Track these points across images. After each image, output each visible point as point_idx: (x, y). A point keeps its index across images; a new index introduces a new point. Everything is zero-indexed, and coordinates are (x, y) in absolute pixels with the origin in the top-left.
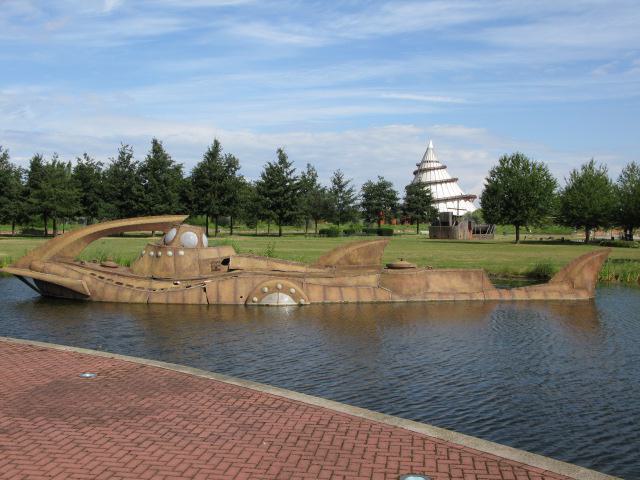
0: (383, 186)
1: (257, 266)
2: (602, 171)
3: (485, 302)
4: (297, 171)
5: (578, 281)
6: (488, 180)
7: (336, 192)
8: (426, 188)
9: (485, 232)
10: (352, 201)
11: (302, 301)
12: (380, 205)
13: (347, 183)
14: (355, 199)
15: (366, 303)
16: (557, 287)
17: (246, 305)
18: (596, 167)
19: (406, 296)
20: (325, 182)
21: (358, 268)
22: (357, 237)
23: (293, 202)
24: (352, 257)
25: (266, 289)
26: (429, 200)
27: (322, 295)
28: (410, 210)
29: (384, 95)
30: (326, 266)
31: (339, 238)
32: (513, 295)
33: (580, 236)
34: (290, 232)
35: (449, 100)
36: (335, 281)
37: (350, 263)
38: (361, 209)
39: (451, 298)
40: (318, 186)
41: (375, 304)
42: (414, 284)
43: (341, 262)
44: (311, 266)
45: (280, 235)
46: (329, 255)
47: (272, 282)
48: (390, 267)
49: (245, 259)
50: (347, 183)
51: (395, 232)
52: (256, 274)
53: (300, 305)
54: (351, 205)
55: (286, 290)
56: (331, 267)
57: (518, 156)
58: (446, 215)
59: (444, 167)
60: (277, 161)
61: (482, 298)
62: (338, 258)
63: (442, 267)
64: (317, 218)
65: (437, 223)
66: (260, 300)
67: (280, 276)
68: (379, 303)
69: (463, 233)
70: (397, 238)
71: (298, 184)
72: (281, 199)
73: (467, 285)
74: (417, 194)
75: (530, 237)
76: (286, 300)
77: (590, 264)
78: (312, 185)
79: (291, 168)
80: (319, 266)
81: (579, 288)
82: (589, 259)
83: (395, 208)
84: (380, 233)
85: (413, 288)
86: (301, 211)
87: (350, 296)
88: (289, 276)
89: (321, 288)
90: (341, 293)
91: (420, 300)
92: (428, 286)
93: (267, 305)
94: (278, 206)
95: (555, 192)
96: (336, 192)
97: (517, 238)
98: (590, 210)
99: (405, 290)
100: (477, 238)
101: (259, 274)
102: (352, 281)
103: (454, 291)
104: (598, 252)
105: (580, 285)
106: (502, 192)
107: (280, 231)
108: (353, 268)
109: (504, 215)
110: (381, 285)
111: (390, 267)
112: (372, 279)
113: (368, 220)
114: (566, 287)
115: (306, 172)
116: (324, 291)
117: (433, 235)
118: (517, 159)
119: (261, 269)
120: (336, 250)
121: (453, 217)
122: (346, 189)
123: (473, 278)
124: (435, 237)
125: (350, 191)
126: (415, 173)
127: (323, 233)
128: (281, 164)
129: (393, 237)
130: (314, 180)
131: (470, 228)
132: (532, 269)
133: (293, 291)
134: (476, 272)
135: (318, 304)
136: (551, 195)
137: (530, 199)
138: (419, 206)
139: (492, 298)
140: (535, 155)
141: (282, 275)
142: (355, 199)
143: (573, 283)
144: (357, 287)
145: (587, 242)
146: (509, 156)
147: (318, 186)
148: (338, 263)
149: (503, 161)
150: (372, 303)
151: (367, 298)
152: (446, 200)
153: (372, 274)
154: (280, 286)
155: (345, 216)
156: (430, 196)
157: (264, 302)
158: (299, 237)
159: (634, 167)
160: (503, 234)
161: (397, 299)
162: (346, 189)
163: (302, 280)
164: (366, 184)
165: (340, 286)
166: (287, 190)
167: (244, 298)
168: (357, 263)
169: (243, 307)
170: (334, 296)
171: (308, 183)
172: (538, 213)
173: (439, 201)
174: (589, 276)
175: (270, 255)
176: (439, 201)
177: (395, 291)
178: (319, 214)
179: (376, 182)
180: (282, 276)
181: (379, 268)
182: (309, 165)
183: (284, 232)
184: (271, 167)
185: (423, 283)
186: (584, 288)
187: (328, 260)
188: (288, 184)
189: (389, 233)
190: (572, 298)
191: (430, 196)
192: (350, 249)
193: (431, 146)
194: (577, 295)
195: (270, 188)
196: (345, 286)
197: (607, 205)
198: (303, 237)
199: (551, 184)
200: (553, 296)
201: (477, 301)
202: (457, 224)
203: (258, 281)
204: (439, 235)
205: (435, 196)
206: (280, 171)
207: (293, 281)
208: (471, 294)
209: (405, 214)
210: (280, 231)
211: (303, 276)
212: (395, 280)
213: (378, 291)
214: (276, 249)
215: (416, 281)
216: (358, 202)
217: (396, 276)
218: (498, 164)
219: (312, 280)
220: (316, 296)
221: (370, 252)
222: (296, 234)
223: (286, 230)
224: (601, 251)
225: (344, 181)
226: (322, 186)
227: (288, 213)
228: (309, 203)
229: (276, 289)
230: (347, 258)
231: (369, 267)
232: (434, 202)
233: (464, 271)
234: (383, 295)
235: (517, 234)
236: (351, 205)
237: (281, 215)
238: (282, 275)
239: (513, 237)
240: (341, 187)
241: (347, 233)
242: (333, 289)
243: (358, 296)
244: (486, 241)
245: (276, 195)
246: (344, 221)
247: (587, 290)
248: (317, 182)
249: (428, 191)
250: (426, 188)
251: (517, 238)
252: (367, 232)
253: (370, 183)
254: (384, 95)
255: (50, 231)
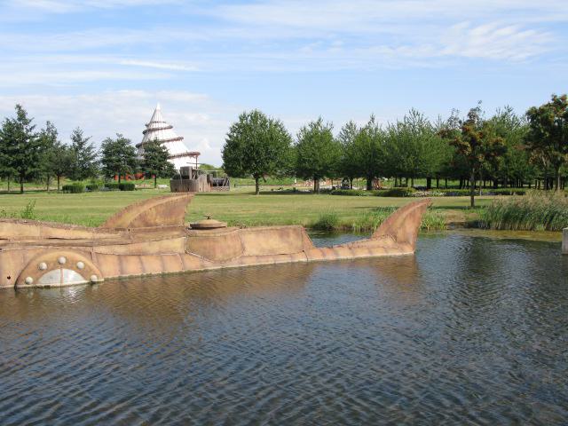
0: (122, 142)
1: (27, 234)
2: (329, 127)
3: (308, 264)
4: (37, 128)
5: (400, 234)
6: (230, 136)
7: (77, 150)
8: (161, 145)
9: (221, 185)
10: (92, 158)
11: (94, 278)
12: (119, 161)
13: (87, 140)
14: (96, 155)
15: (173, 274)
16: (380, 242)
17: (15, 288)
18: (324, 124)
19: (221, 262)
20: (65, 139)
21: (156, 230)
22: (100, 193)
23: (35, 159)
24: (149, 217)
25: (44, 266)
26: (165, 156)
27: (118, 268)
28: (148, 165)
29: (125, 62)
30: (117, 230)
31: (81, 194)
32: (337, 254)
33: (308, 185)
34: (31, 189)
35: (182, 68)
36: (133, 248)
37: (147, 224)
38: (102, 165)
39: (271, 261)
40: (59, 144)
41: (183, 275)
42: (229, 247)
43: (136, 223)
44: (98, 231)
45: (22, 192)
46: (119, 215)
47: (53, 255)
48: (195, 227)
49: (9, 225)
50: (87, 140)
51: (136, 186)
52: (27, 244)
53: (92, 283)
54: (92, 162)
55: (71, 265)
56: (124, 230)
57: (256, 113)
58: (184, 169)
59: (171, 127)
60: (16, 117)
61: (304, 260)
62: (133, 218)
63: (262, 223)
64: (59, 175)
65: (177, 177)
66: (36, 280)
67: (59, 245)
68: (190, 273)
69: (202, 185)
70: (138, 192)
71: (38, 141)
72: (21, 156)
73: (286, 245)
74: (154, 150)
75: (268, 188)
76: (71, 278)
77: (412, 215)
78: (52, 141)
79: (31, 124)
80: (108, 230)
81: (401, 242)
82: (411, 210)
83: (131, 163)
84: (122, 188)
85: (228, 252)
86: (43, 168)
87: (154, 267)
88: (73, 245)
89: (115, 259)
90: (142, 263)
91: (237, 266)
92: (243, 249)
93: (48, 287)
94: (19, 163)
95: (292, 144)
96: (77, 150)
97: (257, 189)
98: (321, 162)
99: (219, 256)
100: (215, 191)
101: (33, 244)
102: (154, 247)
103: (272, 253)
104: (419, 202)
105: (403, 239)
106: (243, 145)
107: (22, 188)
108: (149, 231)
109: (245, 168)
110: (189, 250)
111: (195, 227)
112: (177, 243)
113: (108, 176)
114: (389, 242)
115: (45, 128)
116: (121, 263)
117: (175, 189)
118: (256, 116)
119: (33, 238)
120: (128, 209)
121: (193, 170)
122: (86, 146)
123: (292, 238)
124: (176, 190)
125: (89, 148)
126: (144, 133)
127: (66, 189)
128: (19, 119)
129: (134, 192)
130: (54, 137)
131: (208, 181)
132: (316, 220)
133: (81, 265)
134: (295, 230)
135: (113, 279)
136: (287, 149)
137: (268, 153)
138: (153, 162)
139: (315, 259)
140: (271, 114)
141: (62, 244)
142: (96, 155)
143: (395, 237)
144: (160, 254)
145: (316, 191)
146: (248, 112)
147: (59, 144)
148: (132, 225)
149: (243, 118)
150: (181, 274)
151: (174, 267)
152: (180, 156)
153: (179, 236)
154: (63, 260)
155: (87, 172)
156: (166, 152)
157: (43, 282)
158: (42, 194)
159: (351, 124)
160: (245, 185)
161: (211, 266)
162: (86, 146)
163: (89, 249)
164: (106, 141)
165: (139, 254)
166: (28, 146)
167: (13, 279)
168: (156, 225)
169: (13, 293)
170: (133, 268)
171: (47, 140)
172: (277, 166)
173: (174, 157)
174: (410, 228)
175: (28, 216)
176: (174, 157)
177: (207, 256)
178: (60, 170)
179: (115, 139)
180: (63, 245)
181: (183, 229)
182: (48, 123)
183: (25, 189)
184: (10, 124)
185: (238, 246)
186: (406, 242)
187: (119, 222)
188: (28, 141)
189: (131, 187)
190: (397, 253)
191: (166, 152)
192: (146, 208)
193: (158, 108)
194: (402, 250)
195: (9, 144)
196: (145, 254)
197: (334, 158)
198: (46, 194)
199: (287, 140)
200: (379, 253)
201: (299, 262)
202: (196, 178)
203: (30, 254)
204: (180, 188)
205: (172, 152)
206: (19, 128)
207: (79, 251)
208: (291, 256)
209: (143, 169)
210: (22, 188)
211: (91, 244)
212: (207, 244)
213: (186, 257)
214: (35, 208)
215: (230, 243)
216: (98, 159)
217: (207, 238)
218: (238, 121)
219: (102, 249)
220: (108, 269)
221: (170, 210)
222: (38, 191)
223: (28, 187)
224: (422, 201)
225: (83, 137)
226: (63, 143)
227: (30, 170)
228: (50, 160)
229: (58, 265)
230: (142, 217)
231: (172, 227)
232: (169, 158)
233: (283, 225)
234: (193, 264)
235: (257, 185)
236: (92, 162)
237: (22, 172)
238: (62, 244)
239: (253, 189)
240: (81, 144)
241: (90, 189)
242: (129, 258)
243: (163, 266)
244: (221, 193)
245: (16, 152)
246: (85, 177)
247: (409, 243)
248: (57, 140)
249: (164, 148)
250: (161, 145)
251: (257, 189)
252: (110, 187)
253: (109, 140)
254: (125, 62)
255: (139, 174)
